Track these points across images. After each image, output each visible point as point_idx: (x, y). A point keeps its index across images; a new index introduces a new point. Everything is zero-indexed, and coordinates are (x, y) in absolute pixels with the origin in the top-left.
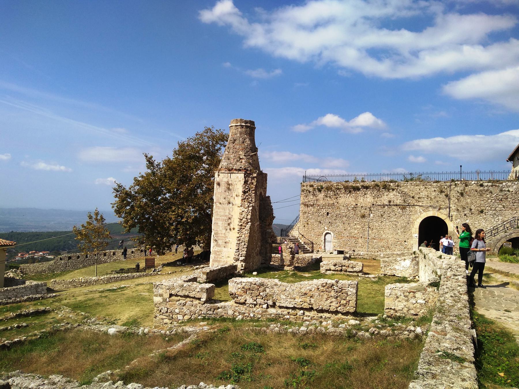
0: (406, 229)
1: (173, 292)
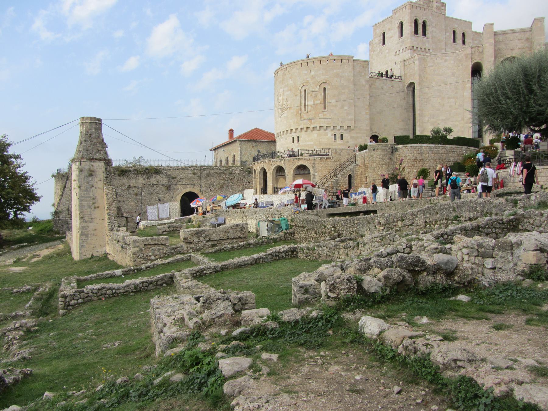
1: (146, 243)
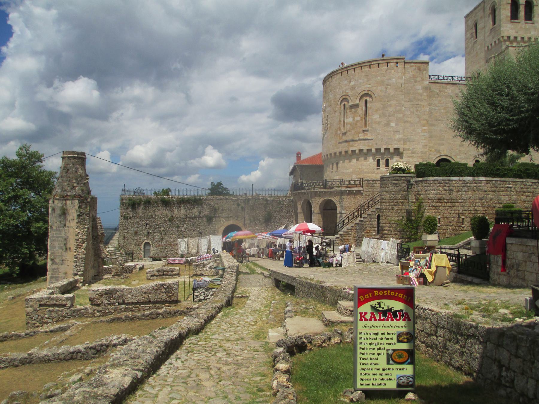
1: (42, 303)
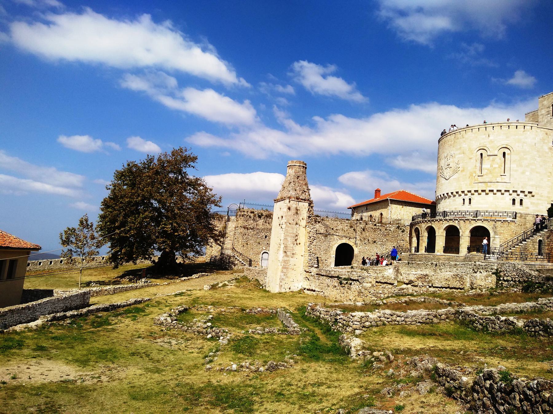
0: (327, 251)
1: (378, 280)
